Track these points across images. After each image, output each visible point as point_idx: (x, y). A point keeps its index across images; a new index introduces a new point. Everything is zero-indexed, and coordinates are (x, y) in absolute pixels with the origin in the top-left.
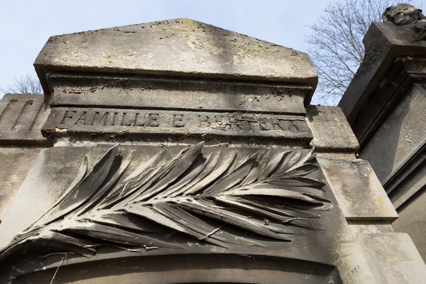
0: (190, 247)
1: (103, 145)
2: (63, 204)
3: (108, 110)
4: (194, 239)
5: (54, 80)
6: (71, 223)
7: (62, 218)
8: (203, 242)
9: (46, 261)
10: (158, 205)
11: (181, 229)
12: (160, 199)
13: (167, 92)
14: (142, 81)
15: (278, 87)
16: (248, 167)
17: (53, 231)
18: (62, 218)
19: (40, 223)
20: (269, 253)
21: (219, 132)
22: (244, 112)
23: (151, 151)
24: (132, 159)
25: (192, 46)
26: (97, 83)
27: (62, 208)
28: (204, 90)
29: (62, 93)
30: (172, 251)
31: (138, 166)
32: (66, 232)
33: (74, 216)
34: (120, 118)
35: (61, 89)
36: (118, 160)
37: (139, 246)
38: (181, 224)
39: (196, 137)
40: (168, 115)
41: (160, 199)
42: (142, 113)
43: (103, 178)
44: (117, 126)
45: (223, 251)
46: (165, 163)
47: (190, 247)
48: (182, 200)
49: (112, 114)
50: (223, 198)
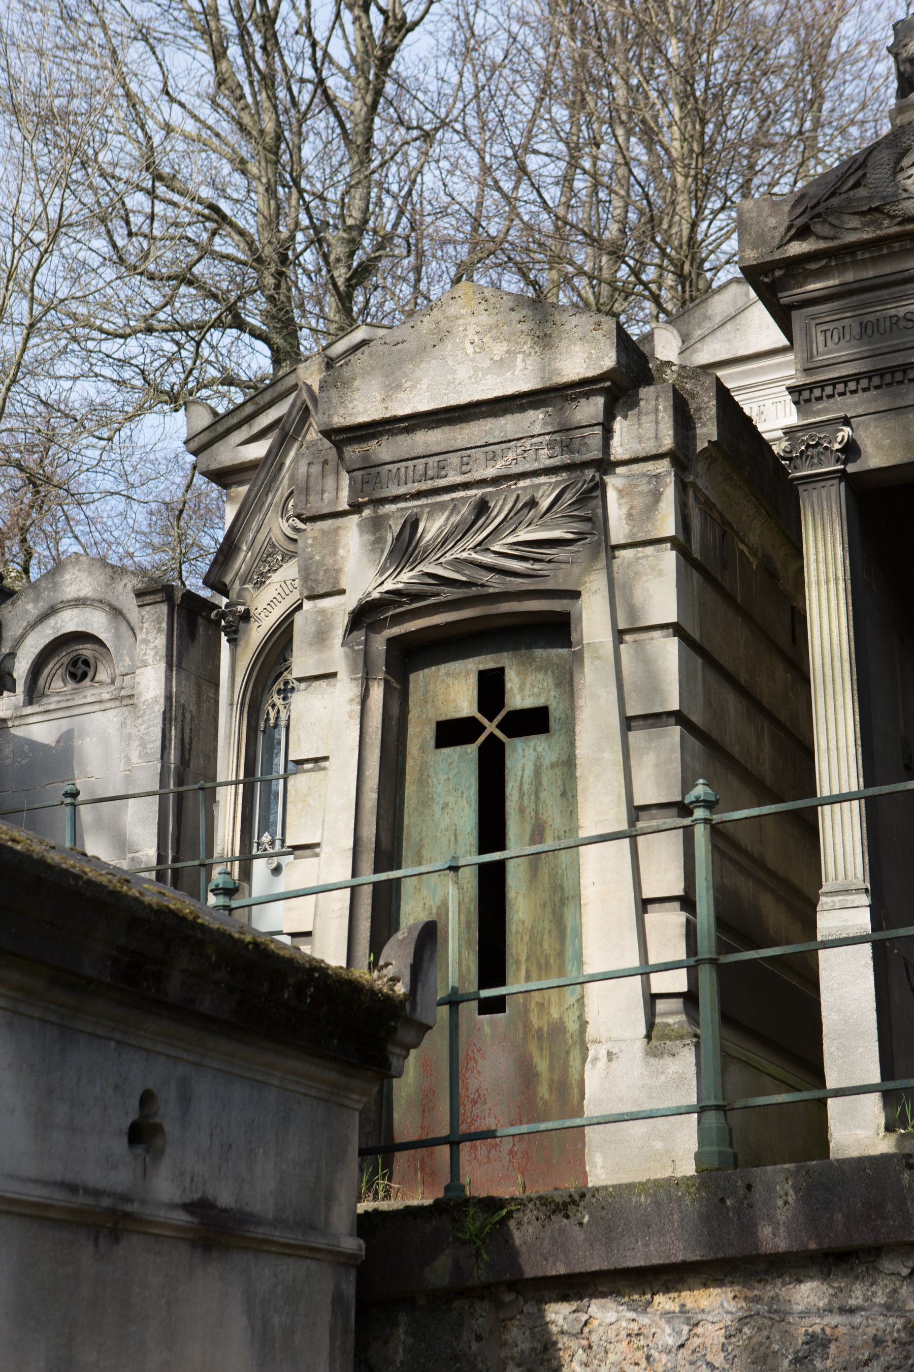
0: (474, 591)
1: (402, 509)
2: (382, 571)
3: (399, 465)
4: (475, 585)
5: (340, 441)
6: (389, 586)
7: (382, 583)
8: (482, 585)
9: (382, 613)
10: (447, 563)
11: (464, 579)
12: (449, 557)
13: (451, 427)
14: (259, 844)
15: (569, 392)
16: (525, 511)
17: (342, 592)
18: (382, 583)
19: (370, 589)
20: (531, 588)
21: (504, 472)
22: (533, 436)
23: (442, 506)
24: (427, 519)
25: (470, 349)
26: (381, 434)
27: (381, 575)
28: (490, 416)
29: (353, 452)
30: (461, 596)
31: (432, 528)
32: (387, 592)
33: (390, 580)
34: (411, 473)
35: (350, 449)
36: (415, 524)
37: (438, 595)
38: (464, 575)
39: (482, 483)
40: (454, 459)
41: (449, 557)
42: (431, 461)
43: (405, 545)
44: (410, 485)
45: (497, 590)
46: (455, 519)
47: (474, 591)
48: (465, 555)
49: (403, 470)
50: (496, 548)
